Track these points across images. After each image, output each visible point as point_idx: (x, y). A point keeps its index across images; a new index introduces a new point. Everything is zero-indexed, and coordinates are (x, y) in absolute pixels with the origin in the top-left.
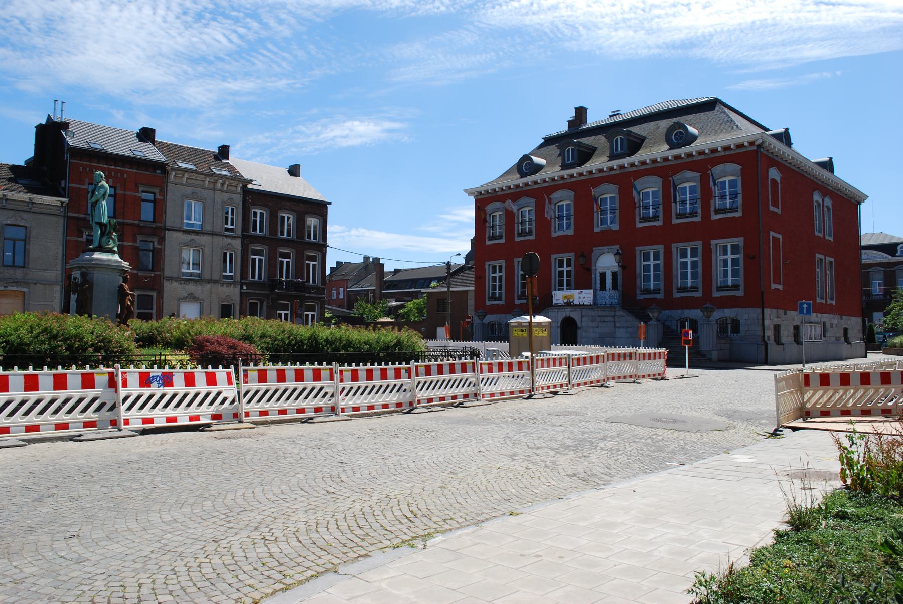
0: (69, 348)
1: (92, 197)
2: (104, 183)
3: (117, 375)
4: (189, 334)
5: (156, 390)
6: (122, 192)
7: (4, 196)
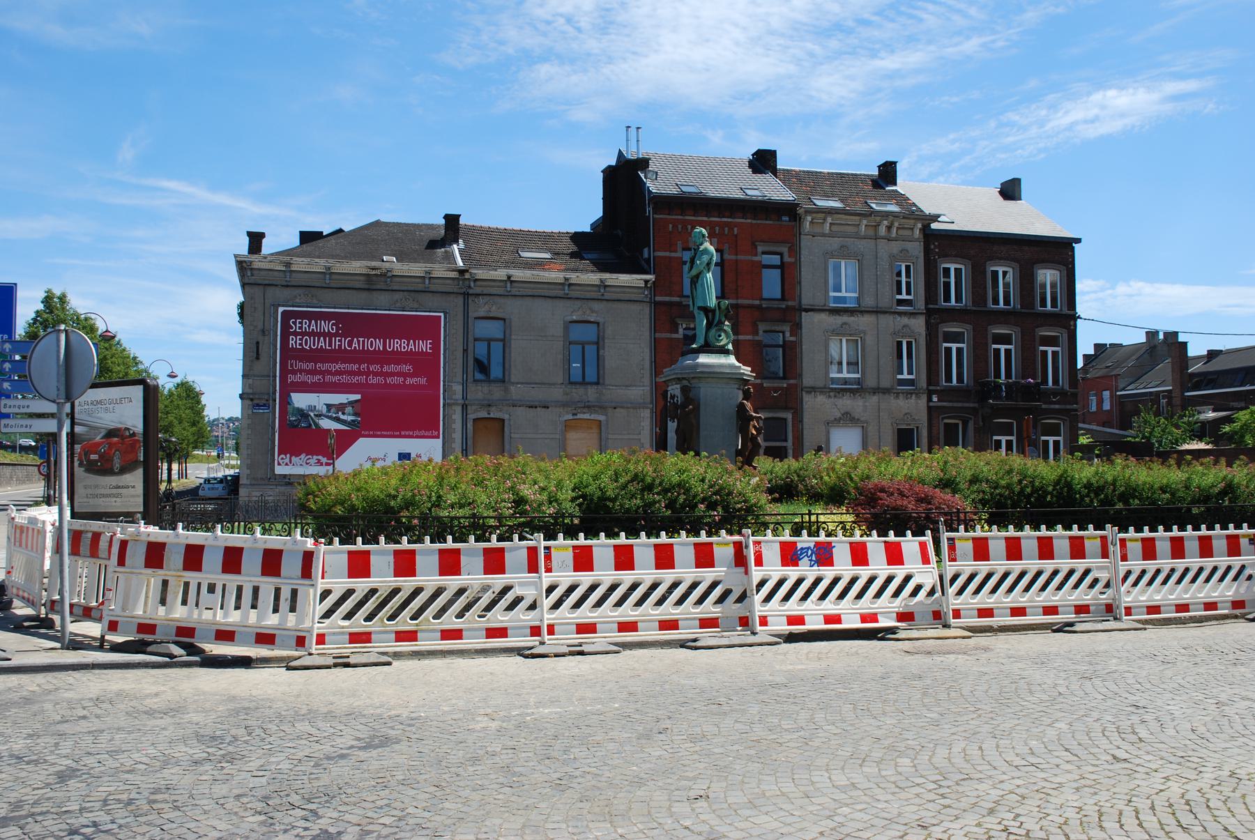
0: (671, 505)
1: (691, 268)
2: (707, 245)
3: (747, 547)
4: (851, 479)
5: (807, 570)
6: (733, 257)
7: (566, 279)
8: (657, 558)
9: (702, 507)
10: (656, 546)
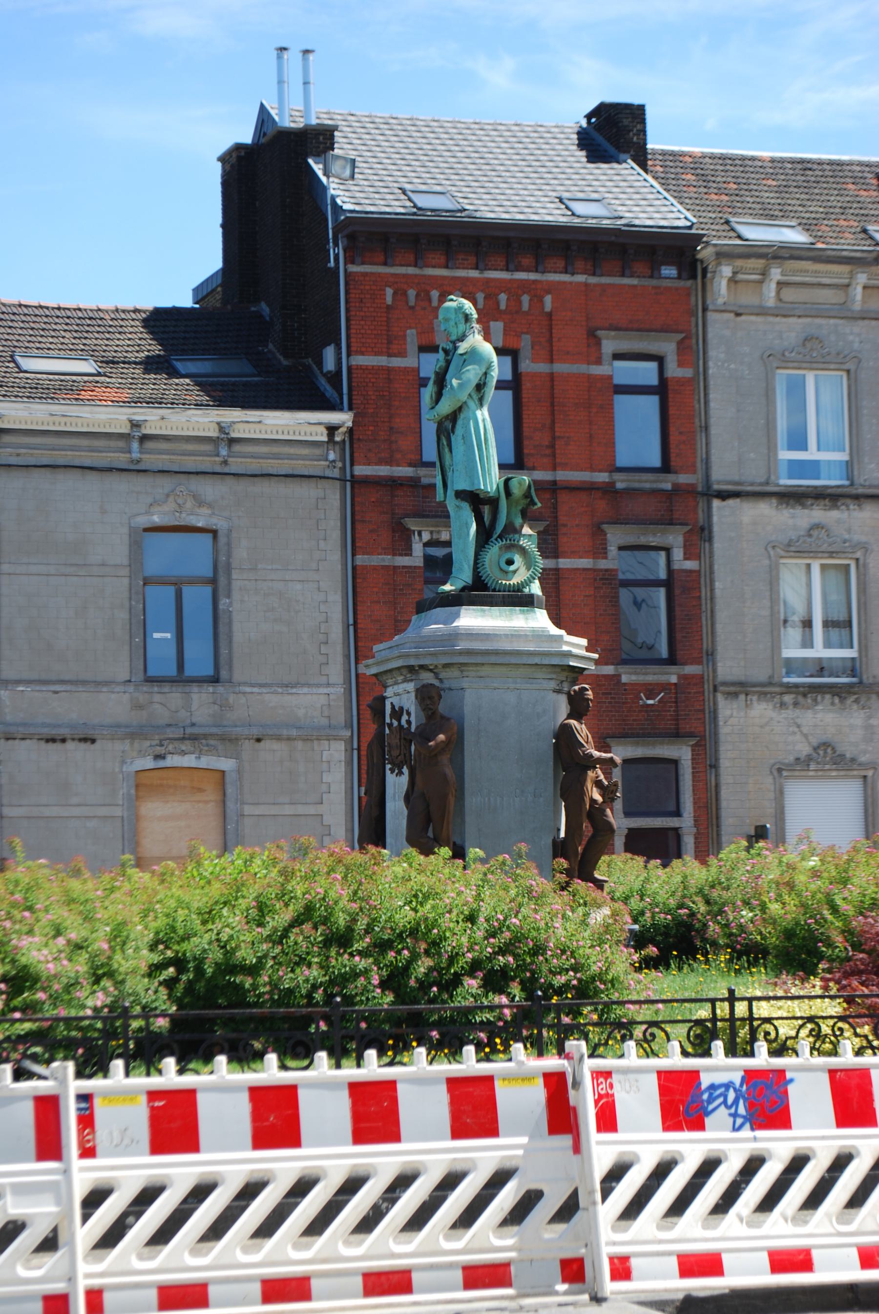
0: (394, 980)
1: (438, 396)
2: (477, 341)
3: (576, 1084)
4: (834, 909)
5: (726, 1140)
6: (542, 368)
7: (135, 425)
8: (358, 1118)
9: (472, 984)
10: (454, 1083)
